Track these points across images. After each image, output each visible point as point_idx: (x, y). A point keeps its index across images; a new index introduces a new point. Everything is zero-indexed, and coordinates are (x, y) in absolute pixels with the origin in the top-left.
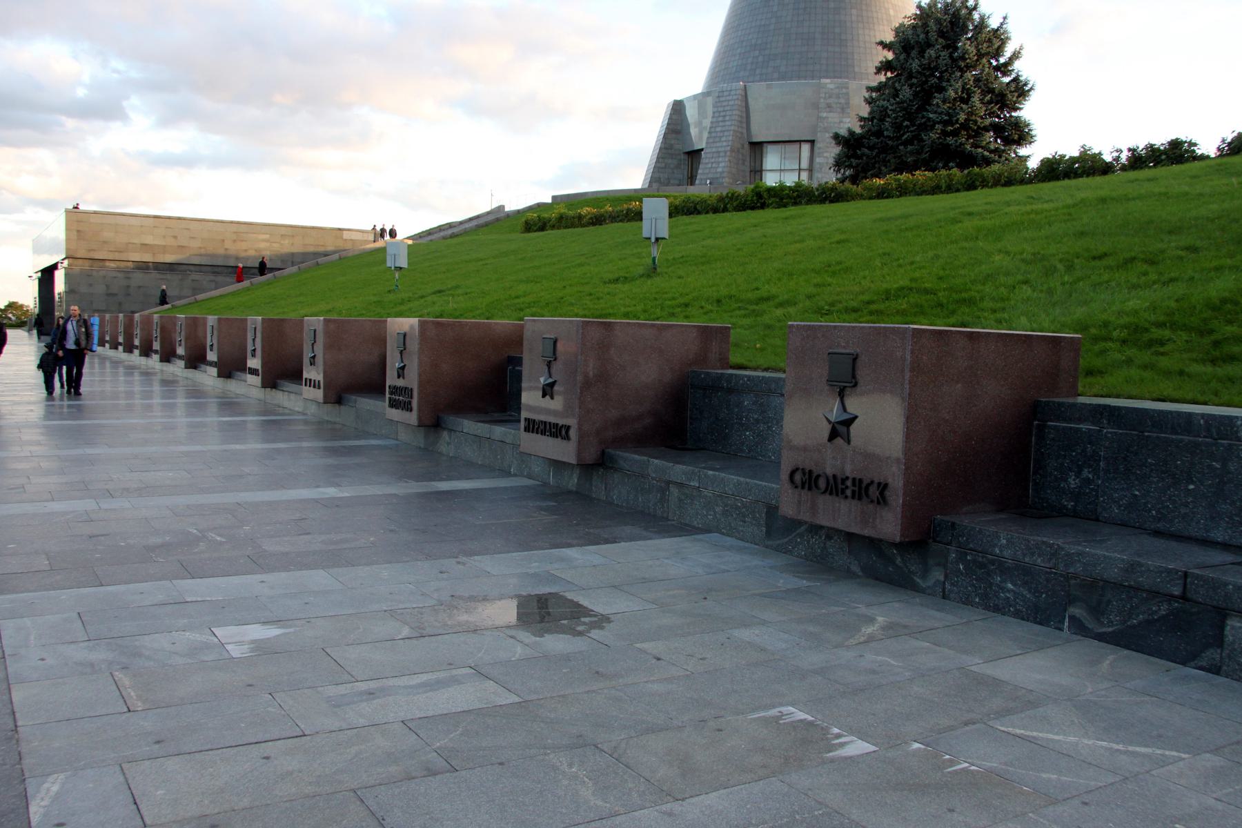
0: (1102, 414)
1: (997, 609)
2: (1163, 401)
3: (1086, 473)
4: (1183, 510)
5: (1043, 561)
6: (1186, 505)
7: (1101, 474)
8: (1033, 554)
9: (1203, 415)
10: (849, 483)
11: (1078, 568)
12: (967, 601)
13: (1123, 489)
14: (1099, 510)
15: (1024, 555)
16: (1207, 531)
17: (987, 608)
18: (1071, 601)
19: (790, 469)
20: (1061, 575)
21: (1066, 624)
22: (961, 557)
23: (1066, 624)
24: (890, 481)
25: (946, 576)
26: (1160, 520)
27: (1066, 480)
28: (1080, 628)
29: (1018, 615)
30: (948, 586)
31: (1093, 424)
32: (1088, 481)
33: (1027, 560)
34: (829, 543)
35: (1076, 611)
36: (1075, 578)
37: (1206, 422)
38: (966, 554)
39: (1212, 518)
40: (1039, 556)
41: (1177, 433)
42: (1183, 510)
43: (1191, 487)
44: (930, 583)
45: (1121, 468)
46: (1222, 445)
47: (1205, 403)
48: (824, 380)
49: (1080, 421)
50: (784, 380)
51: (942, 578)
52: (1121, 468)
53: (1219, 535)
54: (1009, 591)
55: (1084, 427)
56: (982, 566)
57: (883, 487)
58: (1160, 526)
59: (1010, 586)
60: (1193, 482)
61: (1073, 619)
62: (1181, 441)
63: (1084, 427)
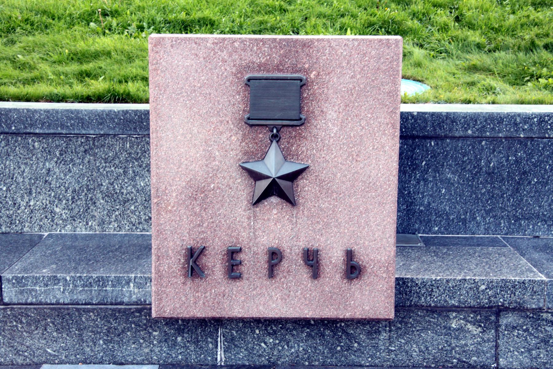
50: (147, 113)
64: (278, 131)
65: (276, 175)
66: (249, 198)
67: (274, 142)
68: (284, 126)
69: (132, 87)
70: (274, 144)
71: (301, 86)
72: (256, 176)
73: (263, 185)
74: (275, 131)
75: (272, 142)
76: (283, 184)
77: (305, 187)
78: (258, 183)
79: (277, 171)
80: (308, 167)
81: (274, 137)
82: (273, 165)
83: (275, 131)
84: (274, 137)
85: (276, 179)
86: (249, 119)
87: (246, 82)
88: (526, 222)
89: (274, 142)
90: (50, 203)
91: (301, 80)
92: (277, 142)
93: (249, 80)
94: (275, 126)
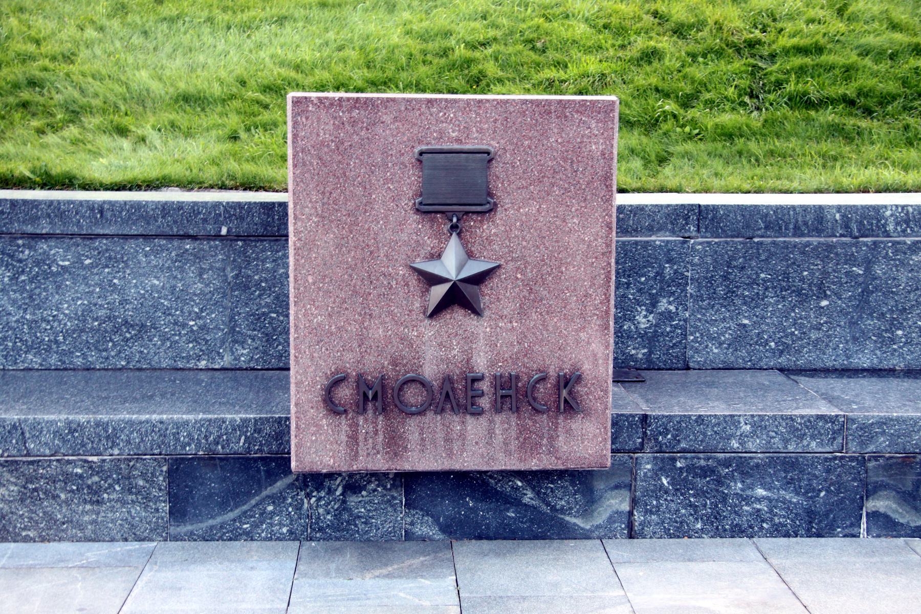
0: (687, 218)
1: (738, 531)
2: (866, 191)
3: (664, 305)
4: (814, 335)
5: (821, 444)
6: (818, 328)
7: (690, 304)
8: (802, 437)
9: (839, 208)
10: (485, 386)
11: (882, 443)
12: (680, 531)
13: (724, 319)
14: (690, 353)
15: (786, 441)
16: (848, 358)
17: (719, 533)
18: (871, 490)
19: (321, 382)
20: (852, 459)
21: (864, 525)
22: (665, 466)
23: (864, 525)
24: (586, 367)
25: (634, 502)
26: (782, 352)
27: (632, 319)
28: (886, 526)
29: (779, 531)
30: (638, 517)
31: (673, 232)
32: (668, 316)
33: (791, 448)
34: (353, 500)
35: (880, 504)
36: (876, 459)
37: (844, 216)
38: (674, 460)
39: (855, 339)
40: (813, 437)
41: (803, 235)
42: (814, 335)
43: (824, 303)
44: (601, 516)
45: (721, 291)
46: (865, 244)
47: (678, 190)
48: (407, 203)
49: (651, 230)
50: (283, 205)
51: (625, 507)
52: (721, 291)
53: (864, 360)
54: (759, 500)
55: (658, 239)
56: (706, 472)
57: (569, 382)
58: (783, 361)
59: (761, 492)
60: (826, 297)
61: (874, 516)
62: (808, 244)
63: (658, 239)
64: (458, 220)
65: (458, 273)
66: (817, 551)
67: (454, 234)
68: (467, 213)
69: (266, 171)
70: (454, 238)
71: (490, 161)
72: (433, 280)
73: (439, 292)
74: (455, 220)
75: (451, 234)
76: (467, 289)
77: (487, 295)
78: (433, 288)
79: (460, 268)
80: (499, 267)
81: (454, 228)
82: (451, 264)
83: (455, 220)
84: (454, 228)
85: (462, 286)
86: (421, 203)
87: (416, 156)
88: (52, 252)
89: (454, 234)
90: (712, 219)
91: (488, 153)
92: (459, 235)
93: (421, 153)
94: (454, 212)
